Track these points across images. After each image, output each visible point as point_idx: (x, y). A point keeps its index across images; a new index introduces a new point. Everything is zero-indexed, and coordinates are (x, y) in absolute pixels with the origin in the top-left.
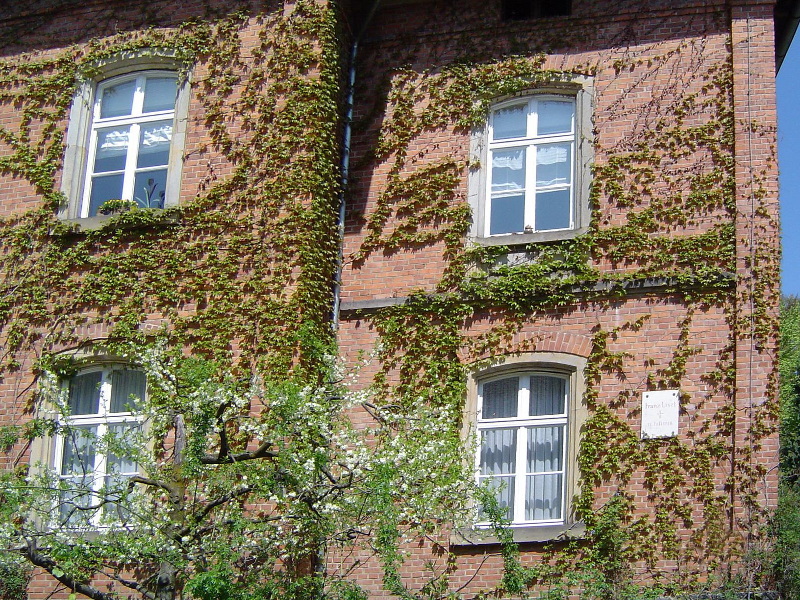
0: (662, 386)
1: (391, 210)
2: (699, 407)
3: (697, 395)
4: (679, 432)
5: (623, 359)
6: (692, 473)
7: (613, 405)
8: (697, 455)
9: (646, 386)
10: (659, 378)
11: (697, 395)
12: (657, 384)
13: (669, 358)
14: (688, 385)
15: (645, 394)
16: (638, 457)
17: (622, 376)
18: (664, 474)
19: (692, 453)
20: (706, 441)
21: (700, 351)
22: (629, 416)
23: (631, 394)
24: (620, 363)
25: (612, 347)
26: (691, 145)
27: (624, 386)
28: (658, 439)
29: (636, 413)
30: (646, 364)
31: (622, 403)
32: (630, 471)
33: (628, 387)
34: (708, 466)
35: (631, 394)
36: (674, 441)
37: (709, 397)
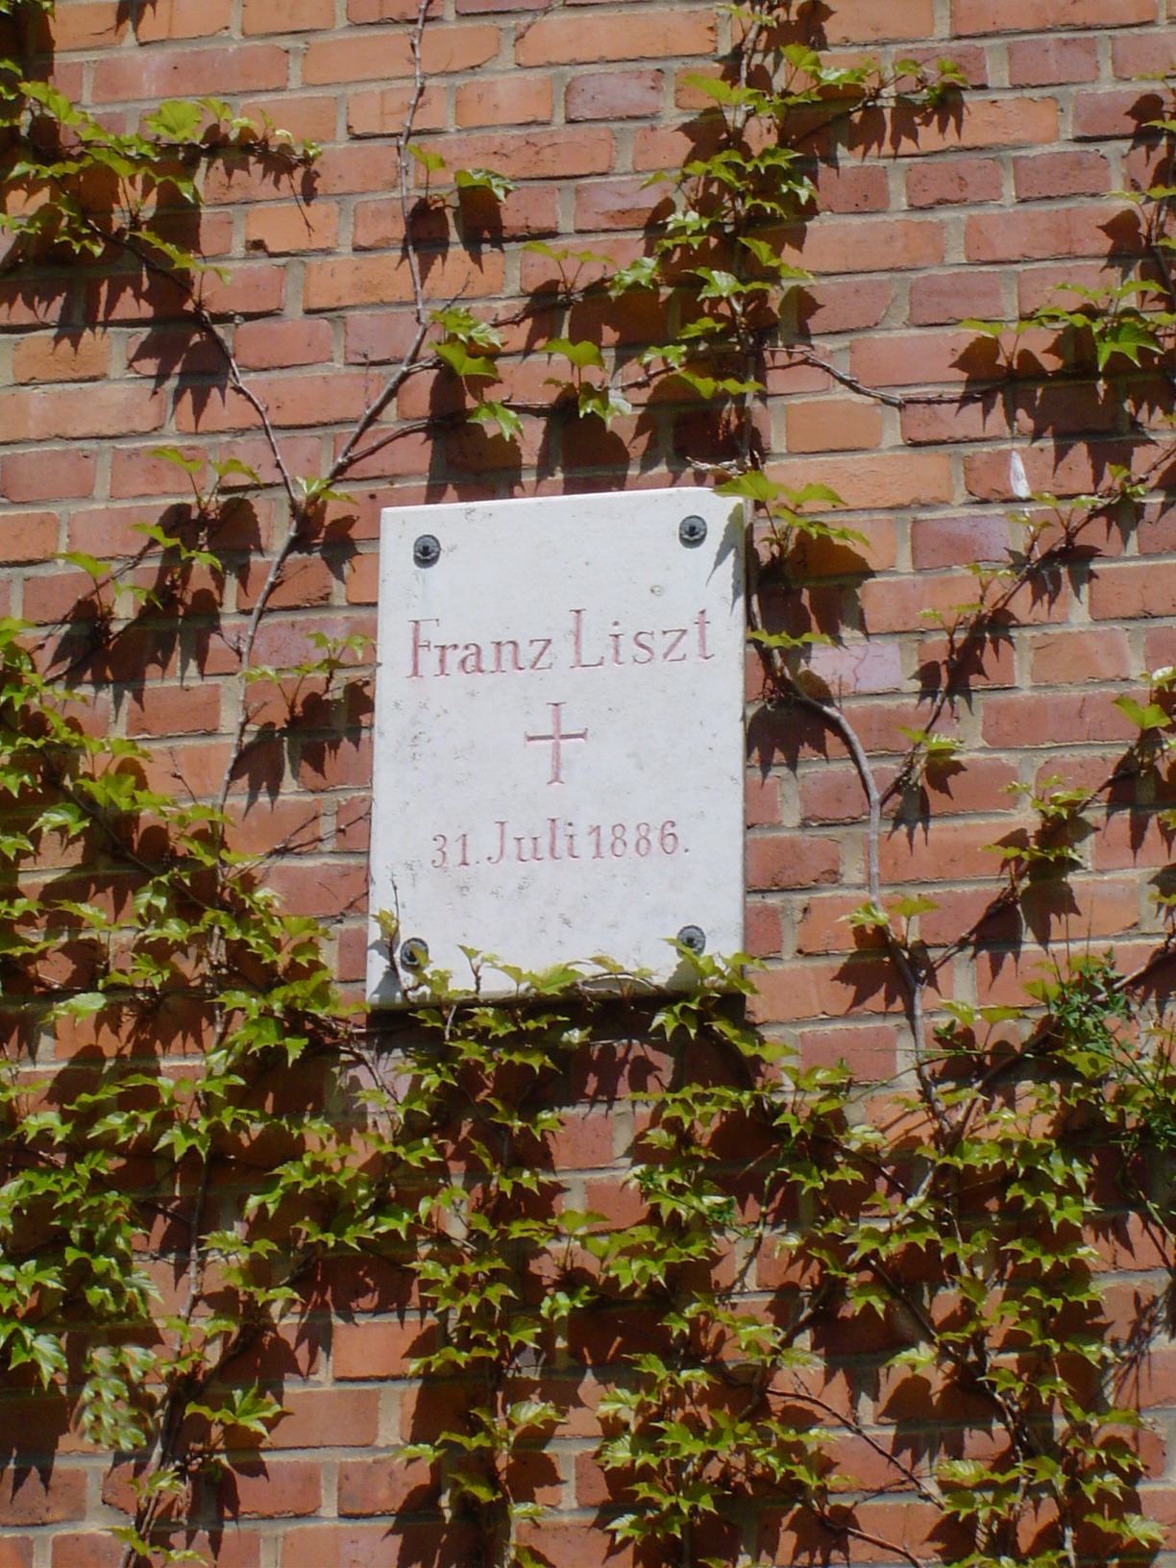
0: (584, 455)
1: (309, 1478)
2: (954, 674)
3: (937, 549)
4: (760, 933)
5: (203, 182)
6: (909, 1407)
7: (95, 648)
8: (964, 1196)
9: (418, 453)
10: (558, 364)
11: (937, 549)
12: (531, 436)
13: (649, 168)
14: (841, 449)
15: (401, 524)
16: (330, 1207)
17: (191, 350)
18: (622, 1404)
19: (903, 1167)
20: (1050, 1038)
21: (947, 104)
22: (258, 763)
23: (277, 530)
24: (180, 221)
25: (110, 83)
26: (474, 356)
27: (203, 454)
28: (532, 1005)
29: (323, 727)
30: (424, 231)
31: (177, 622)
32: (256, 1359)
33: (251, 458)
34: (1083, 1323)
35: (277, 530)
36: (700, 1026)
37: (1059, 565)
